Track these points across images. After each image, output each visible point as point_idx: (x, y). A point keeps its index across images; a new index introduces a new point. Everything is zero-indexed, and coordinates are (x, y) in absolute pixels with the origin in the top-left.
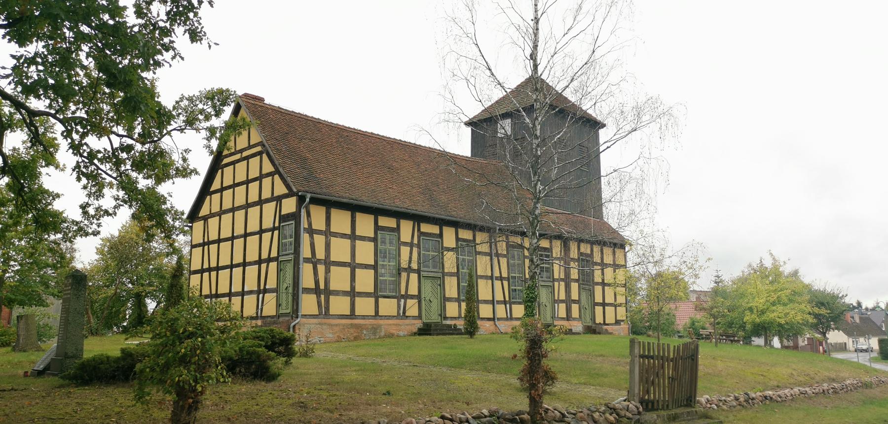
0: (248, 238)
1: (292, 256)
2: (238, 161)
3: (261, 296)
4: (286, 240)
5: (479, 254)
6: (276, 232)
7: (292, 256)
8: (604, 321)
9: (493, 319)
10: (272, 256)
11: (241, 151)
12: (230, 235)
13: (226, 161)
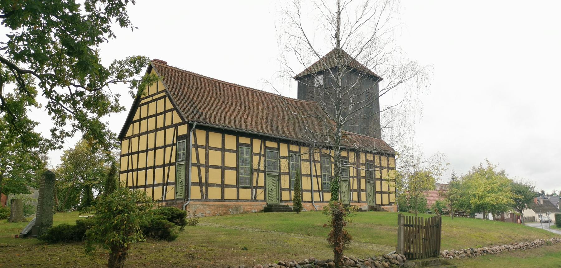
0: (157, 151)
1: (185, 162)
2: (151, 102)
3: (165, 187)
4: (181, 152)
5: (303, 161)
6: (175, 147)
7: (185, 162)
8: (382, 203)
9: (312, 202)
10: (172, 162)
11: (152, 96)
12: (145, 149)
13: (143, 102)
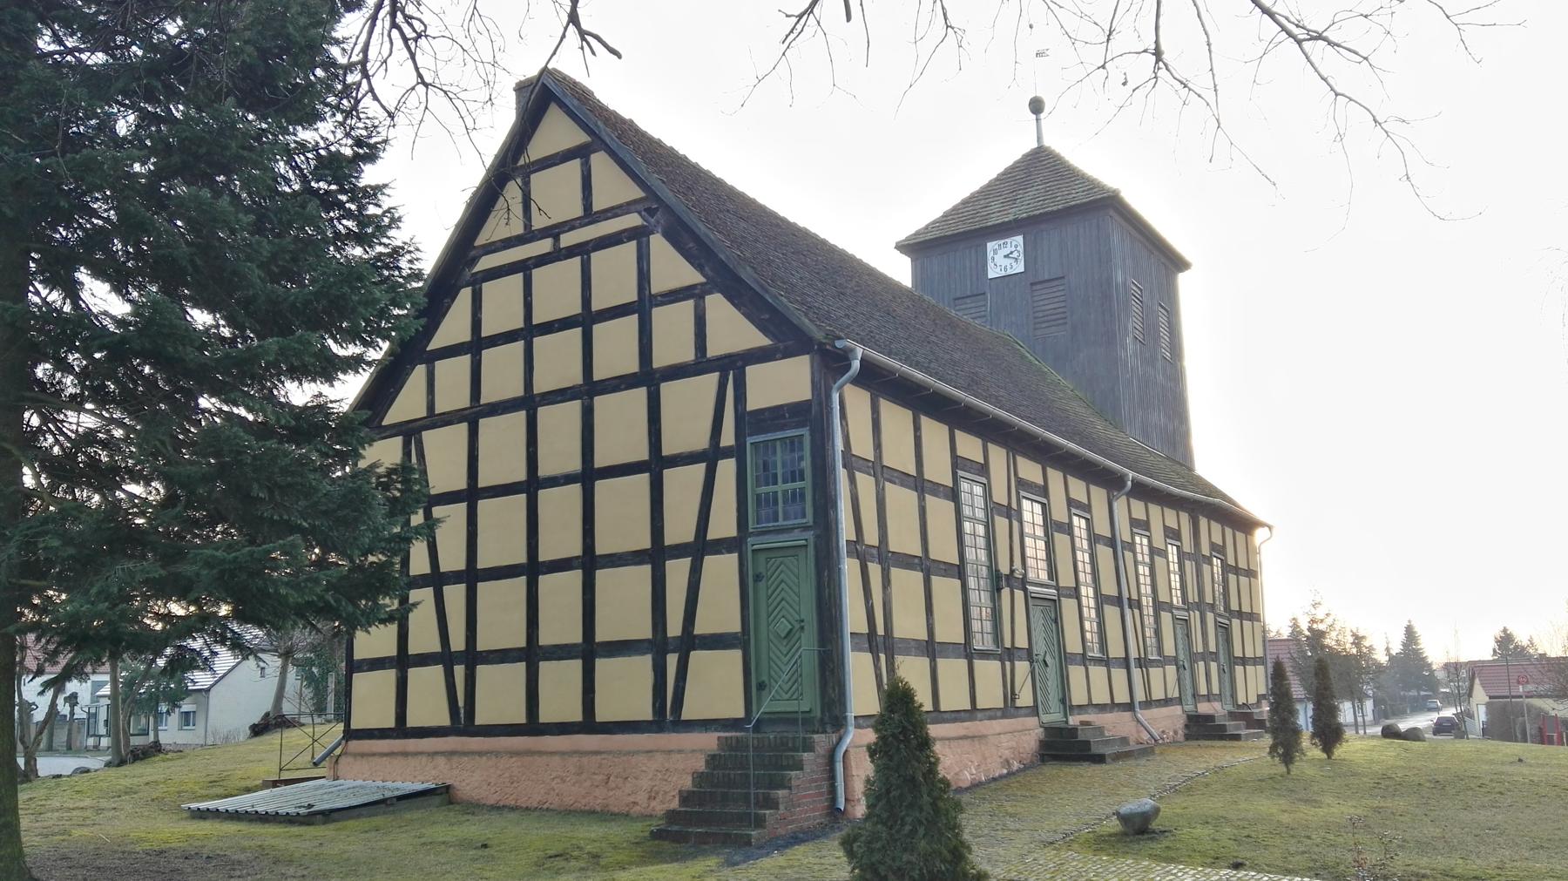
0: (598, 329)
1: (810, 535)
2: (542, 260)
3: (672, 660)
4: (771, 488)
5: (52, 746)
6: (727, 469)
7: (810, 535)
8: (1090, 699)
9: (1129, 707)
10: (713, 533)
11: (554, 232)
12: (485, 424)
13: (487, 263)
